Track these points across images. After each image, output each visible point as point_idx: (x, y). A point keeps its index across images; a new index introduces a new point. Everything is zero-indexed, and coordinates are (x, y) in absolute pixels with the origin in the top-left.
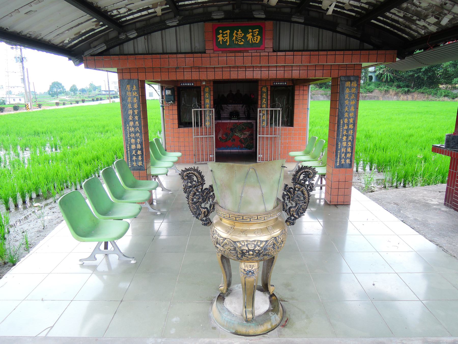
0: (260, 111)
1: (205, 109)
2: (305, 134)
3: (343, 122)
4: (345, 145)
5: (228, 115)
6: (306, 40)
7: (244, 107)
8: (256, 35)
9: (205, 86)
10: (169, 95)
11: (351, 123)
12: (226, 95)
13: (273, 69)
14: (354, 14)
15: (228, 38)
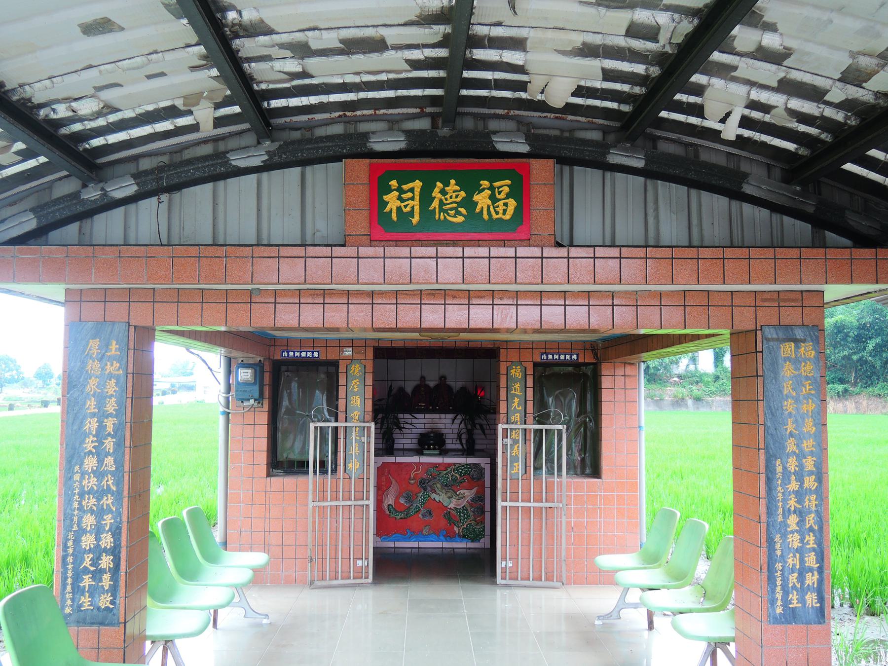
0: (505, 431)
1: (348, 424)
2: (635, 500)
3: (785, 468)
4: (796, 544)
5: (415, 441)
6: (651, 220)
7: (457, 421)
8: (502, 196)
9: (351, 360)
10: (246, 383)
11: (811, 473)
12: (409, 389)
13: (553, 302)
14: (790, 146)
15: (416, 203)
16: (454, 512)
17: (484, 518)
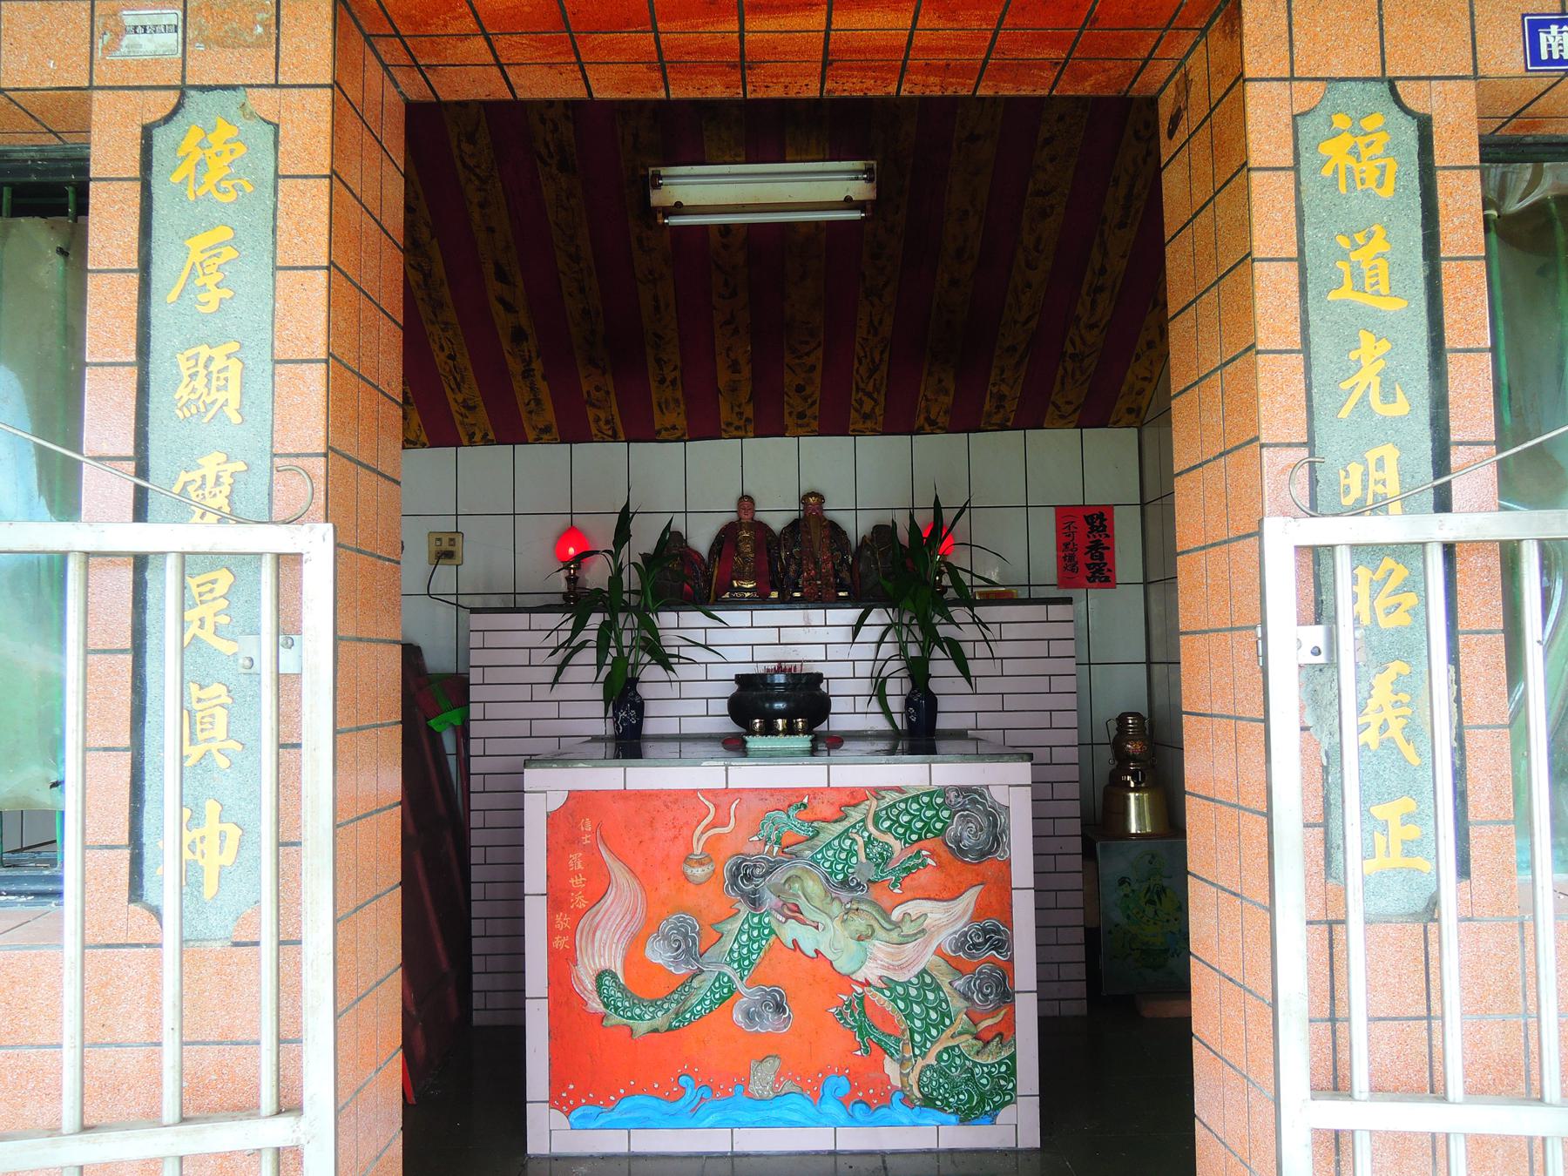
0: (1316, 559)
5: (722, 707)
7: (869, 634)
12: (701, 538)
16: (881, 999)
17: (1009, 1023)
